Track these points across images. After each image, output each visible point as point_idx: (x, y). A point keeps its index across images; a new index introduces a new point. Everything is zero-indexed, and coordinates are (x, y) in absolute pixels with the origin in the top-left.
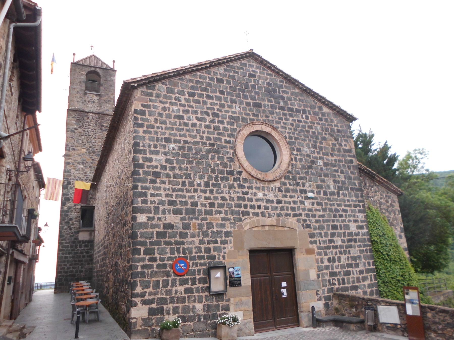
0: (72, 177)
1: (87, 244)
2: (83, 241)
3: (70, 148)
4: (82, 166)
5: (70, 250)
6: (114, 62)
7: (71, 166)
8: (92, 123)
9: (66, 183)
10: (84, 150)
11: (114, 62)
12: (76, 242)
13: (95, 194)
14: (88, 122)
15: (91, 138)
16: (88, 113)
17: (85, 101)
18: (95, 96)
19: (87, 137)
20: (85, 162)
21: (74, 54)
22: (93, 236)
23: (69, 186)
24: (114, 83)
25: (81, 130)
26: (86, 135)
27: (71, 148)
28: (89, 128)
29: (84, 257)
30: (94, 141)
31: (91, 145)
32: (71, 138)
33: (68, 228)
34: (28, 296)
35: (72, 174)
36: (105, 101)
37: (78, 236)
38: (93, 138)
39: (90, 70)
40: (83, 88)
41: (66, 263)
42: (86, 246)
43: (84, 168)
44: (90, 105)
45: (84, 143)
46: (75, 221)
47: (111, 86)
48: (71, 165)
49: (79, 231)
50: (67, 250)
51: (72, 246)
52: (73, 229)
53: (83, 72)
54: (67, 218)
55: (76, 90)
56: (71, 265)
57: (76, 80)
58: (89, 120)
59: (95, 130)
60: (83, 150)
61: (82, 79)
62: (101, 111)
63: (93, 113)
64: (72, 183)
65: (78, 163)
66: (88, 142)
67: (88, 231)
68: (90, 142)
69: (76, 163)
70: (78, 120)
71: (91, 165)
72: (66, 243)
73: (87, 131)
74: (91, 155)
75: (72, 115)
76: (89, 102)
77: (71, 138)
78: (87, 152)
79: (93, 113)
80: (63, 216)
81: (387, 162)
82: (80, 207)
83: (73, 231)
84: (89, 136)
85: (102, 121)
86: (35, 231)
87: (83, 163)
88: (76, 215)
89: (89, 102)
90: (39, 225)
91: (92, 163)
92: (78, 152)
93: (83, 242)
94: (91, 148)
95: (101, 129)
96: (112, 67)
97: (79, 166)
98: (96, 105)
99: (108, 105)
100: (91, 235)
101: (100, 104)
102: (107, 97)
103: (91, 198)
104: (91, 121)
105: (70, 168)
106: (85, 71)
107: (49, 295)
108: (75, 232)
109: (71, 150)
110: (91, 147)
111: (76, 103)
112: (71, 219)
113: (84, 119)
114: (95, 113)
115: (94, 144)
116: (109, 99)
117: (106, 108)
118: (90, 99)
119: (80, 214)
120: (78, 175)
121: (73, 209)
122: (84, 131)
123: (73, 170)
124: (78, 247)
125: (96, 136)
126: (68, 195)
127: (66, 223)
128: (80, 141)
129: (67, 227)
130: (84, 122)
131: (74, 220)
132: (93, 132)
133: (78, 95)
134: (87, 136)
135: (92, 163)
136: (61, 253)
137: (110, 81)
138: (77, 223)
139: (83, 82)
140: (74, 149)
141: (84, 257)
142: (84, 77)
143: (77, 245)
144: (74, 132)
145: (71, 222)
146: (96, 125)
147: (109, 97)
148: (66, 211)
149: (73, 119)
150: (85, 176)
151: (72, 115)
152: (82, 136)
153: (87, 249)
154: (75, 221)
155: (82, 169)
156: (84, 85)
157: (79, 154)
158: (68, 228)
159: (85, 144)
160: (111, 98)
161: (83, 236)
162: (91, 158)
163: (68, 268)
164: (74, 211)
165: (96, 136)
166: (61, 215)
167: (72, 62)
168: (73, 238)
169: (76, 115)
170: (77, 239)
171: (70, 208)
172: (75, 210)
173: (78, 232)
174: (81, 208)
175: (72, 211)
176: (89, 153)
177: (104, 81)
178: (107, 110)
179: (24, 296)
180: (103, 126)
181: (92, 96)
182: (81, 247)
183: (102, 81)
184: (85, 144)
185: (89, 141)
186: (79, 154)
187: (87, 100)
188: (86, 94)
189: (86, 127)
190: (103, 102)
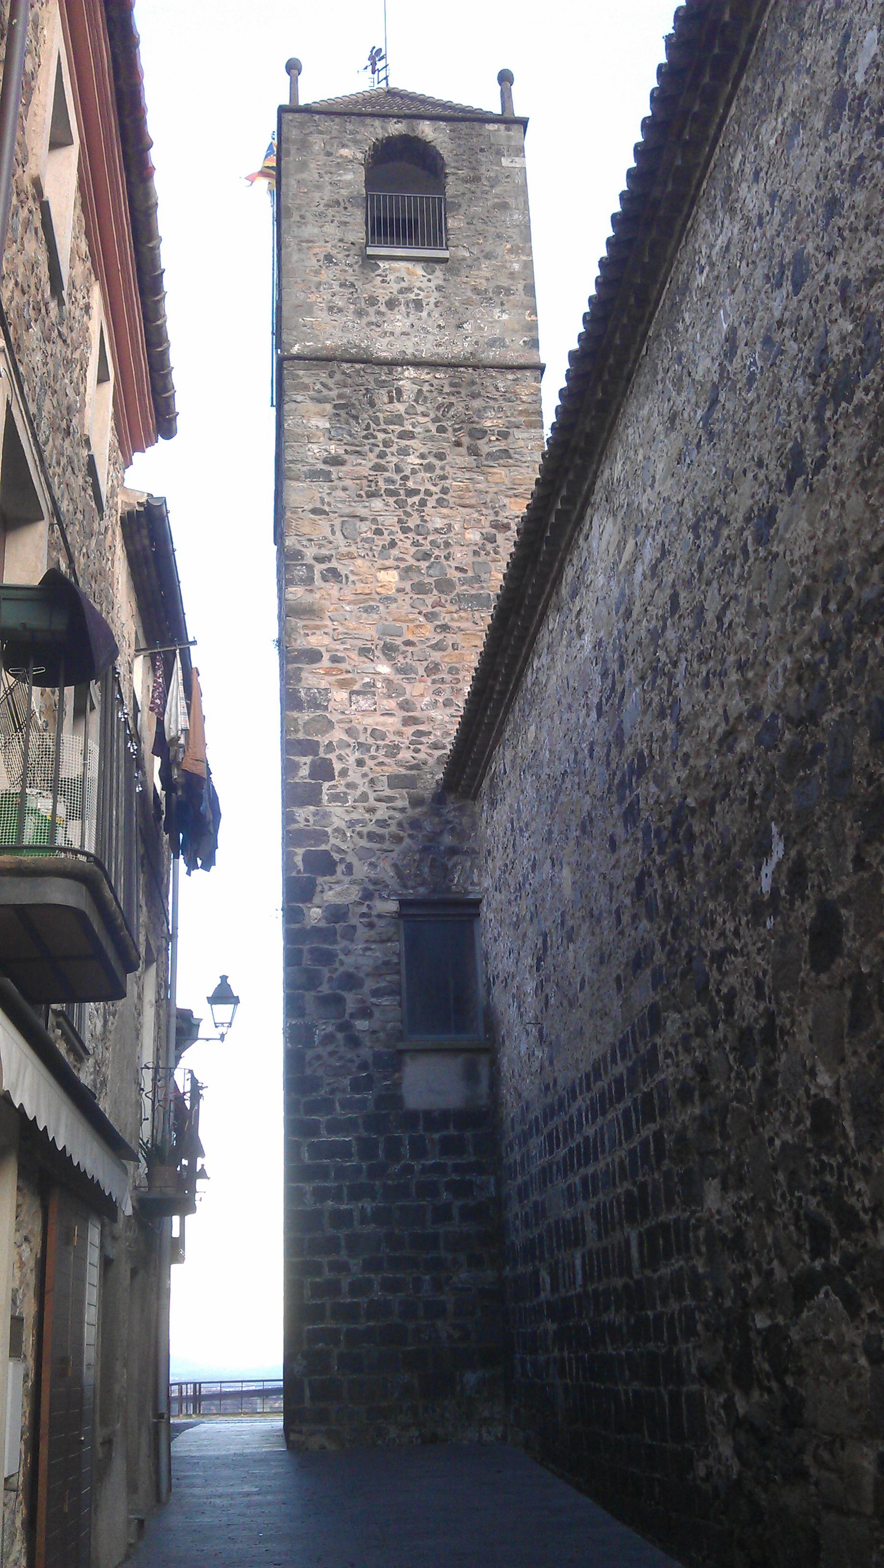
0: (337, 735)
1: (452, 1131)
2: (427, 1113)
3: (310, 568)
4: (384, 669)
5: (358, 1170)
6: (505, 78)
7: (328, 673)
8: (423, 423)
9: (304, 771)
10: (391, 578)
11: (505, 78)
12: (387, 1117)
13: (474, 826)
14: (398, 419)
15: (423, 503)
16: (392, 364)
17: (372, 301)
18: (419, 270)
19: (401, 504)
20: (398, 641)
21: (293, 68)
22: (484, 1086)
23: (326, 785)
24: (522, 190)
25: (364, 467)
26: (391, 493)
27: (319, 568)
28: (404, 452)
29: (442, 1214)
30: (439, 523)
31: (427, 547)
32: (314, 511)
33: (340, 1036)
34: (144, 1464)
35: (334, 717)
36: (475, 290)
37: (398, 1084)
38: (431, 502)
39: (381, 134)
40: (358, 233)
41: (343, 1256)
42: (449, 1146)
43: (397, 678)
44: (399, 321)
45: (387, 538)
46: (376, 993)
47: (504, 206)
48: (326, 662)
49: (401, 1052)
50: (341, 1173)
51: (367, 1149)
52: (367, 1041)
53: (345, 152)
54: (326, 972)
55: (321, 249)
56: (372, 1265)
57: (317, 195)
58: (400, 408)
59: (441, 456)
60: (383, 576)
61: (349, 184)
62: (462, 348)
63: (417, 364)
64: (337, 766)
65: (364, 652)
66: (405, 530)
67: (455, 1051)
68: (418, 530)
69: (354, 655)
70: (345, 411)
71: (436, 656)
72: (333, 1128)
73: (398, 469)
74: (430, 599)
75: (306, 387)
76: (391, 304)
77: (314, 511)
78: (407, 586)
79: (417, 364)
80: (306, 960)
81: (730, 16)
82: (392, 906)
83: (366, 1052)
84: (415, 492)
85: (477, 404)
86: (158, 1026)
87: (389, 651)
88: (378, 953)
89: (391, 304)
90: (182, 1002)
91: (438, 647)
92: (360, 587)
93: (435, 1120)
94: (424, 564)
95: (474, 451)
96: (497, 110)
97: (368, 666)
98: (431, 317)
99: (497, 313)
100: (470, 1075)
101: (451, 310)
102: (485, 269)
103: (453, 851)
104: (411, 411)
105: (323, 684)
106: (356, 142)
107: (263, 1460)
108: (377, 1056)
109: (318, 581)
110: (426, 556)
111: (323, 316)
112: (351, 981)
113: (372, 404)
114: (432, 365)
115: (440, 539)
116: (505, 282)
117: (488, 333)
118: (395, 287)
119: (396, 946)
120: (370, 721)
121: (354, 921)
122: (377, 468)
123: (340, 696)
124: (405, 1150)
125: (445, 491)
126: (322, 836)
127: (324, 1001)
128: (364, 526)
129: (330, 1029)
130: (376, 421)
131: (370, 984)
132: (430, 468)
133: (326, 275)
134: (400, 495)
135: (438, 647)
136: (308, 1187)
137: (494, 182)
138: (385, 1001)
139: (351, 199)
140: (333, 575)
141: (442, 1214)
142: (354, 178)
143: (398, 1141)
144: (327, 476)
145: (351, 1000)
146: (441, 430)
147: (498, 269)
148: (317, 931)
149: (312, 407)
150: (408, 721)
151: (306, 387)
152: (371, 495)
153: (456, 1168)
154: (376, 993)
155: (388, 681)
156: (358, 216)
157: (367, 605)
158: (340, 1036)
159: (393, 544)
160: (512, 275)
161: (430, 1083)
162: (430, 617)
163: (356, 1288)
164: (362, 933)
165: (445, 491)
166: (292, 958)
167: (286, 101)
168: (369, 1096)
169: (330, 382)
170: (392, 1098)
171: (337, 914)
172: (371, 925)
173: (393, 1061)
174: (400, 915)
175: (350, 933)
176: (420, 588)
177: (462, 188)
178: (492, 343)
179: (119, 1466)
180: (484, 433)
181: (404, 270)
182: (418, 1150)
183: (453, 187)
184: (393, 544)
185: (411, 524)
186: (367, 605)
187: (383, 295)
188: (369, 262)
189: (387, 444)
190: (467, 302)
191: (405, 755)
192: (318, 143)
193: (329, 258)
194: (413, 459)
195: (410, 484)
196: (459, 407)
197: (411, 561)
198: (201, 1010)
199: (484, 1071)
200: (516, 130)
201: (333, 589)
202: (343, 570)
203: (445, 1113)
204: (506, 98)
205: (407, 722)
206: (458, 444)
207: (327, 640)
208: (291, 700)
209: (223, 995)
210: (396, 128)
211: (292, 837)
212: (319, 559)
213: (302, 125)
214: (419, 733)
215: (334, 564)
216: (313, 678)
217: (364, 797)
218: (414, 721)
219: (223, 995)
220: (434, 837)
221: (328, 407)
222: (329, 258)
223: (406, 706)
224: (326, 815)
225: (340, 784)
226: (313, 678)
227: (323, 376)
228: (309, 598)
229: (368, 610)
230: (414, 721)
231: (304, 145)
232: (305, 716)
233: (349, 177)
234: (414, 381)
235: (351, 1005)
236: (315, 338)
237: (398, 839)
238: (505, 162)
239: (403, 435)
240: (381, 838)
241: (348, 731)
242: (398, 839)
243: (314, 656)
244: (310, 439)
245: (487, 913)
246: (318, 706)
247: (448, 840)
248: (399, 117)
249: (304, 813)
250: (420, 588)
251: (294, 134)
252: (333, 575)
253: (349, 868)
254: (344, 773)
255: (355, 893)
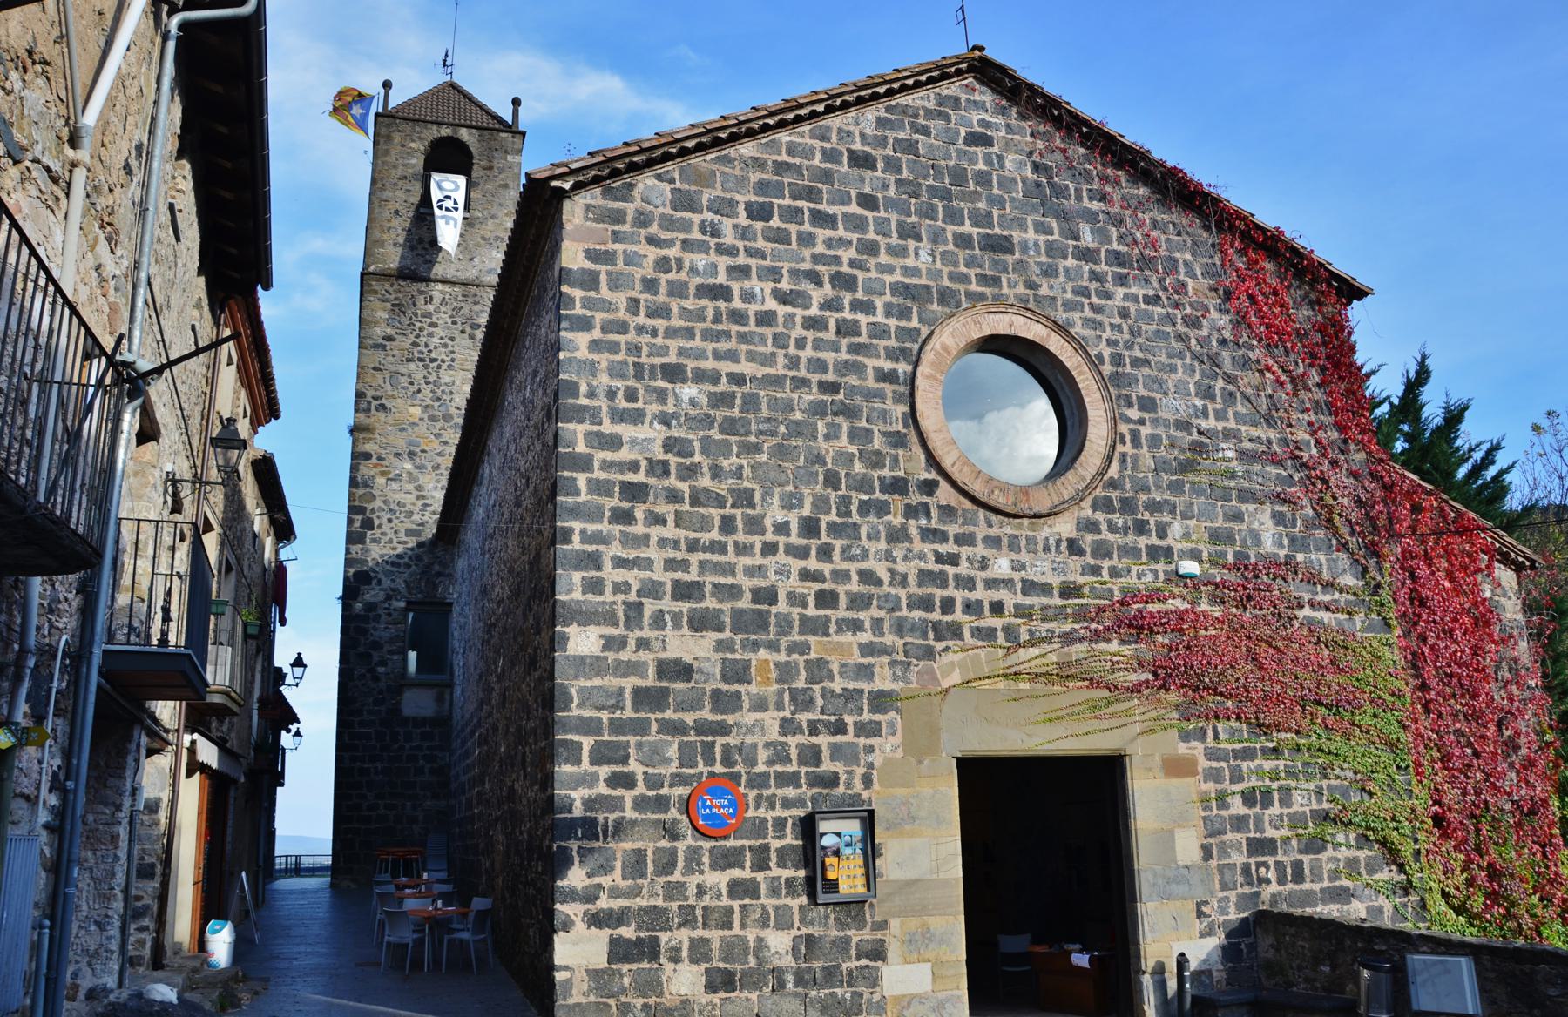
0: (378, 503)
2: (415, 719)
4: (408, 466)
6: (516, 102)
7: (375, 466)
8: (443, 318)
9: (357, 524)
11: (516, 102)
13: (453, 561)
14: (429, 315)
15: (439, 367)
19: (426, 367)
20: (418, 450)
22: (447, 705)
27: (374, 403)
28: (431, 335)
30: (447, 380)
35: (377, 493)
36: (483, 238)
37: (399, 703)
38: (444, 366)
39: (436, 135)
45: (416, 387)
48: (374, 460)
53: (413, 145)
58: (431, 308)
59: (452, 339)
60: (412, 410)
61: (414, 166)
64: (376, 522)
66: (427, 383)
70: (398, 308)
73: (426, 345)
75: (376, 292)
78: (425, 416)
83: (382, 685)
84: (433, 360)
87: (412, 454)
90: (277, 663)
97: (399, 464)
100: (440, 699)
103: (439, 574)
104: (437, 310)
106: (421, 139)
110: (438, 399)
120: (398, 497)
122: (415, 344)
123: (381, 481)
125: (453, 360)
128: (403, 379)
130: (416, 315)
132: (445, 346)
144: (384, 347)
145: (376, 656)
146: (454, 323)
149: (378, 304)
151: (376, 292)
152: (409, 360)
154: (391, 652)
155: (410, 473)
159: (419, 391)
162: (437, 436)
177: (482, 173)
184: (419, 391)
185: (431, 380)
190: (477, 245)
191: (416, 517)
192: (397, 138)
193: (397, 212)
194: (436, 340)
195: (433, 355)
196: (466, 310)
197: (429, 402)
198: (287, 669)
199: (447, 697)
200: (518, 139)
201: (382, 415)
202: (388, 405)
203: (424, 719)
204: (515, 114)
205: (418, 498)
206: (463, 332)
207: (376, 447)
208: (353, 483)
209: (299, 662)
210: (446, 131)
211: (349, 562)
212: (375, 398)
213: (389, 125)
214: (426, 505)
215: (383, 401)
216: (366, 469)
217: (391, 541)
218: (423, 497)
219: (299, 662)
220: (429, 566)
221: (388, 305)
222: (397, 212)
223: (419, 488)
224: (368, 550)
225: (377, 532)
226: (366, 469)
227: (387, 286)
228: (367, 421)
229: (402, 430)
230: (423, 497)
231: (389, 138)
232: (360, 492)
233: (414, 161)
234: (441, 292)
235: (376, 659)
236: (384, 262)
237: (408, 566)
238: (509, 158)
239: (431, 325)
240: (398, 565)
241: (384, 502)
242: (408, 566)
243: (368, 456)
244: (376, 324)
245: (456, 609)
246: (367, 486)
247: (437, 568)
248: (449, 125)
249: (356, 548)
250: (433, 419)
251: (383, 131)
252: (383, 407)
253: (379, 582)
254: (380, 526)
255: (382, 596)
